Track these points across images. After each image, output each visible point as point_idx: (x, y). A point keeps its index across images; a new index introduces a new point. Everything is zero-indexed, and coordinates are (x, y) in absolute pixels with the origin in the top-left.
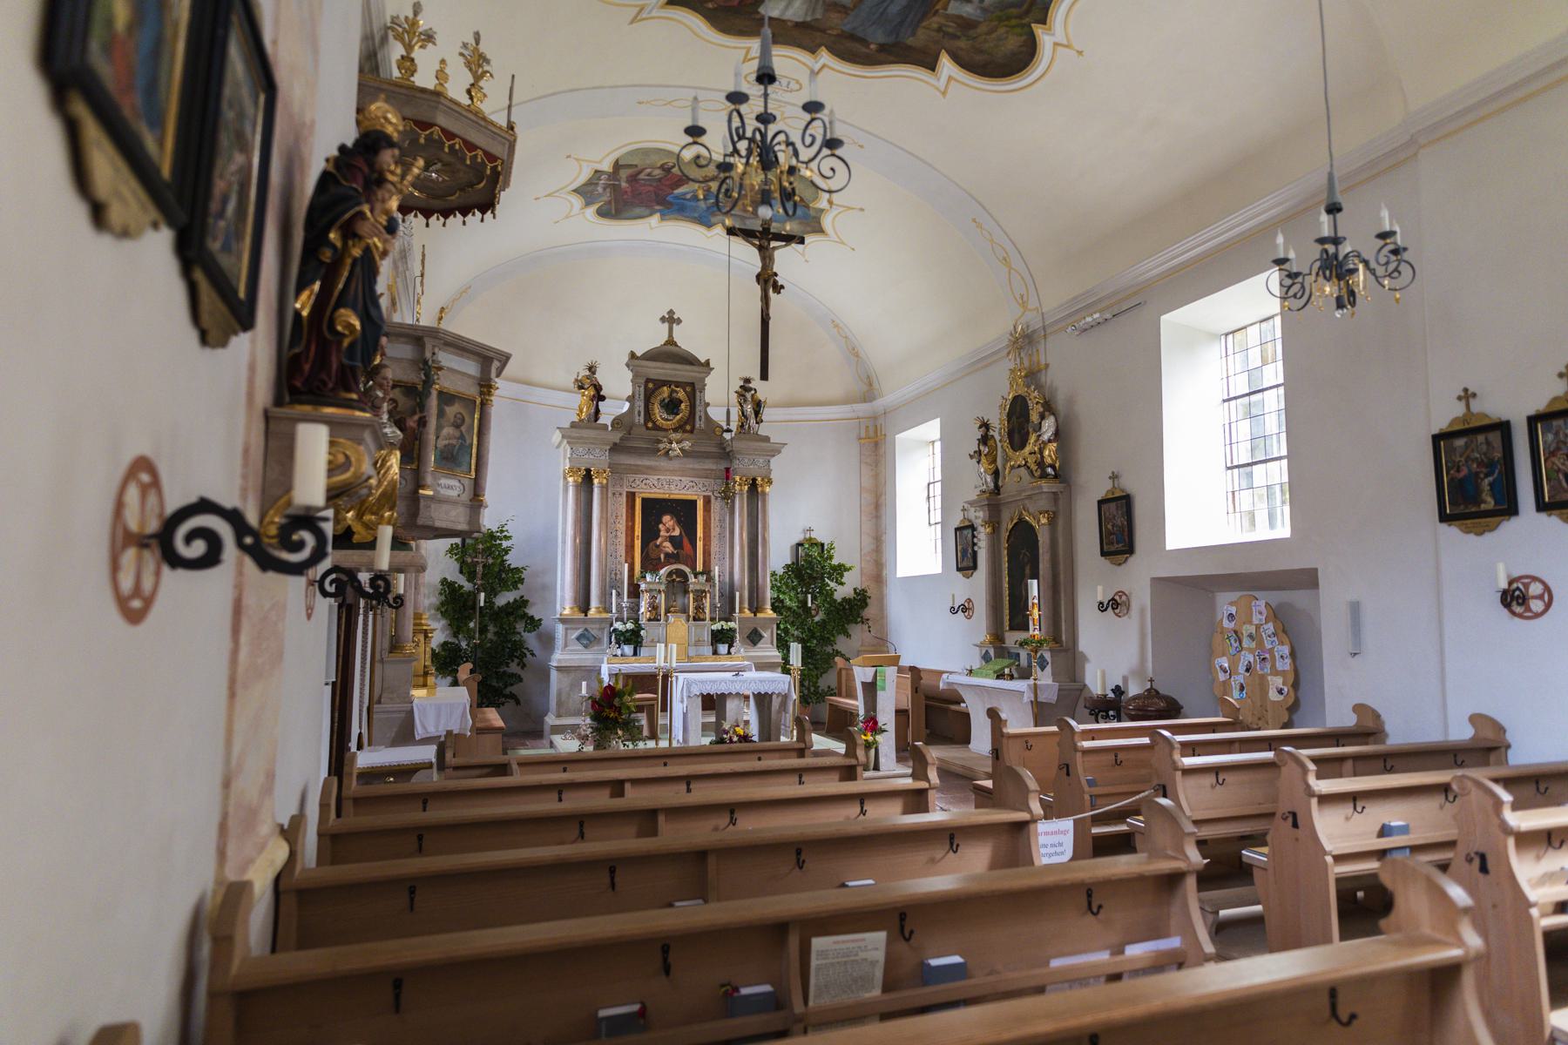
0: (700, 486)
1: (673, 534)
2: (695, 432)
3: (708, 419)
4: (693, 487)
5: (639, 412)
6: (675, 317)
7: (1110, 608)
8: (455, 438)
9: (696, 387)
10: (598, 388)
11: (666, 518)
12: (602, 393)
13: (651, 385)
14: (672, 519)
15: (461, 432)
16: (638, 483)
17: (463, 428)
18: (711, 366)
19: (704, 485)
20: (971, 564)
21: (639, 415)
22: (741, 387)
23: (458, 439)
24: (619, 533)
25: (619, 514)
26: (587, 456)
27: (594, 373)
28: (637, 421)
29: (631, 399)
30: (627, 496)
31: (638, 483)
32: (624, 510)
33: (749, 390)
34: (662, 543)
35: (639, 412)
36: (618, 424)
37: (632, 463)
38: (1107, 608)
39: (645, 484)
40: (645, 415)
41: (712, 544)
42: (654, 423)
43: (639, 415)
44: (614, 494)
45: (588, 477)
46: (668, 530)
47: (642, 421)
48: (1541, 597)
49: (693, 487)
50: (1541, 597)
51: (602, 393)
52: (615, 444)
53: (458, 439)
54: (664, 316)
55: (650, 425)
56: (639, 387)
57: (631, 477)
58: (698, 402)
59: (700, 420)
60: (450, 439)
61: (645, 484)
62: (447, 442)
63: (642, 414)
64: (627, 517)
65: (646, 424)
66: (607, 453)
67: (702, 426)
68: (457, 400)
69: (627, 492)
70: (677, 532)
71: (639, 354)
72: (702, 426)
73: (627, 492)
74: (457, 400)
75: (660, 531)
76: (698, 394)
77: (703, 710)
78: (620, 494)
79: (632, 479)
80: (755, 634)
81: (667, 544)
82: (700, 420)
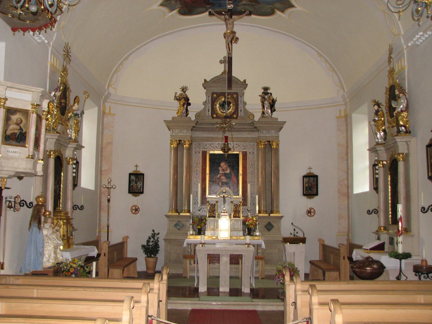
0: (241, 147)
1: (226, 172)
2: (238, 118)
3: (246, 111)
4: (237, 147)
5: (209, 110)
6: (223, 60)
7: (373, 213)
8: (17, 129)
9: (239, 95)
10: (187, 99)
11: (223, 164)
12: (189, 102)
13: (215, 96)
14: (226, 164)
15: (20, 126)
16: (208, 146)
17: (22, 125)
18: (247, 83)
19: (243, 146)
20: (131, 191)
21: (209, 111)
22: (263, 93)
23: (19, 130)
24: (198, 172)
25: (198, 163)
26: (180, 134)
27: (185, 92)
28: (207, 114)
29: (204, 103)
30: (202, 153)
31: (208, 146)
32: (201, 160)
33: (267, 94)
34: (220, 177)
35: (209, 110)
36: (198, 116)
37: (205, 136)
38: (427, 211)
39: (212, 147)
40: (212, 111)
41: (248, 176)
42: (217, 115)
43: (209, 111)
44: (196, 152)
45: (180, 143)
46: (223, 170)
47: (210, 114)
48: (313, 212)
49: (237, 147)
50: (313, 212)
51: (189, 102)
52: (194, 127)
53: (19, 130)
54: (221, 60)
55: (235, 116)
56: (209, 97)
57: (205, 143)
58: (239, 103)
59: (241, 112)
60: (14, 130)
61: (212, 147)
62: (12, 132)
63: (239, 110)
64: (202, 164)
65: (212, 116)
66: (190, 132)
67: (242, 115)
68: (18, 112)
69: (202, 151)
70: (228, 171)
71: (208, 80)
72: (242, 115)
73: (202, 151)
74: (18, 112)
75: (219, 170)
76: (239, 98)
77: (230, 264)
78: (199, 152)
79: (204, 145)
80: (269, 225)
81: (223, 177)
82: (241, 112)
